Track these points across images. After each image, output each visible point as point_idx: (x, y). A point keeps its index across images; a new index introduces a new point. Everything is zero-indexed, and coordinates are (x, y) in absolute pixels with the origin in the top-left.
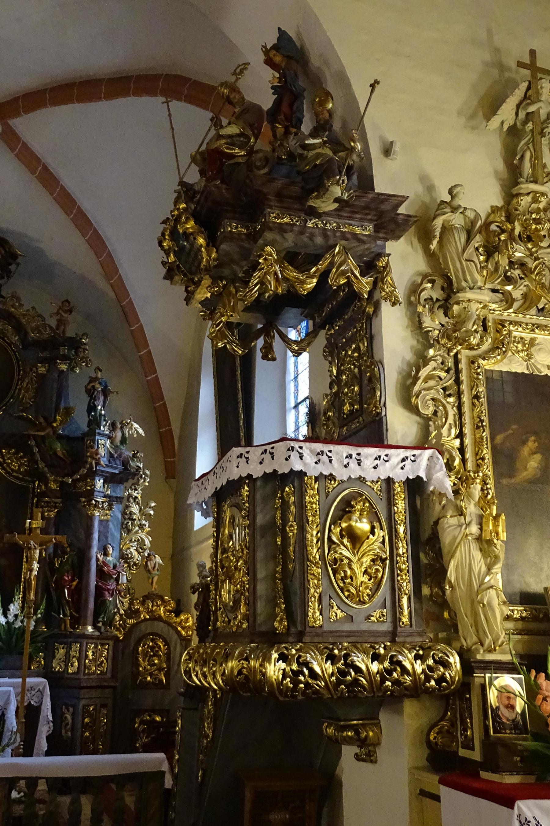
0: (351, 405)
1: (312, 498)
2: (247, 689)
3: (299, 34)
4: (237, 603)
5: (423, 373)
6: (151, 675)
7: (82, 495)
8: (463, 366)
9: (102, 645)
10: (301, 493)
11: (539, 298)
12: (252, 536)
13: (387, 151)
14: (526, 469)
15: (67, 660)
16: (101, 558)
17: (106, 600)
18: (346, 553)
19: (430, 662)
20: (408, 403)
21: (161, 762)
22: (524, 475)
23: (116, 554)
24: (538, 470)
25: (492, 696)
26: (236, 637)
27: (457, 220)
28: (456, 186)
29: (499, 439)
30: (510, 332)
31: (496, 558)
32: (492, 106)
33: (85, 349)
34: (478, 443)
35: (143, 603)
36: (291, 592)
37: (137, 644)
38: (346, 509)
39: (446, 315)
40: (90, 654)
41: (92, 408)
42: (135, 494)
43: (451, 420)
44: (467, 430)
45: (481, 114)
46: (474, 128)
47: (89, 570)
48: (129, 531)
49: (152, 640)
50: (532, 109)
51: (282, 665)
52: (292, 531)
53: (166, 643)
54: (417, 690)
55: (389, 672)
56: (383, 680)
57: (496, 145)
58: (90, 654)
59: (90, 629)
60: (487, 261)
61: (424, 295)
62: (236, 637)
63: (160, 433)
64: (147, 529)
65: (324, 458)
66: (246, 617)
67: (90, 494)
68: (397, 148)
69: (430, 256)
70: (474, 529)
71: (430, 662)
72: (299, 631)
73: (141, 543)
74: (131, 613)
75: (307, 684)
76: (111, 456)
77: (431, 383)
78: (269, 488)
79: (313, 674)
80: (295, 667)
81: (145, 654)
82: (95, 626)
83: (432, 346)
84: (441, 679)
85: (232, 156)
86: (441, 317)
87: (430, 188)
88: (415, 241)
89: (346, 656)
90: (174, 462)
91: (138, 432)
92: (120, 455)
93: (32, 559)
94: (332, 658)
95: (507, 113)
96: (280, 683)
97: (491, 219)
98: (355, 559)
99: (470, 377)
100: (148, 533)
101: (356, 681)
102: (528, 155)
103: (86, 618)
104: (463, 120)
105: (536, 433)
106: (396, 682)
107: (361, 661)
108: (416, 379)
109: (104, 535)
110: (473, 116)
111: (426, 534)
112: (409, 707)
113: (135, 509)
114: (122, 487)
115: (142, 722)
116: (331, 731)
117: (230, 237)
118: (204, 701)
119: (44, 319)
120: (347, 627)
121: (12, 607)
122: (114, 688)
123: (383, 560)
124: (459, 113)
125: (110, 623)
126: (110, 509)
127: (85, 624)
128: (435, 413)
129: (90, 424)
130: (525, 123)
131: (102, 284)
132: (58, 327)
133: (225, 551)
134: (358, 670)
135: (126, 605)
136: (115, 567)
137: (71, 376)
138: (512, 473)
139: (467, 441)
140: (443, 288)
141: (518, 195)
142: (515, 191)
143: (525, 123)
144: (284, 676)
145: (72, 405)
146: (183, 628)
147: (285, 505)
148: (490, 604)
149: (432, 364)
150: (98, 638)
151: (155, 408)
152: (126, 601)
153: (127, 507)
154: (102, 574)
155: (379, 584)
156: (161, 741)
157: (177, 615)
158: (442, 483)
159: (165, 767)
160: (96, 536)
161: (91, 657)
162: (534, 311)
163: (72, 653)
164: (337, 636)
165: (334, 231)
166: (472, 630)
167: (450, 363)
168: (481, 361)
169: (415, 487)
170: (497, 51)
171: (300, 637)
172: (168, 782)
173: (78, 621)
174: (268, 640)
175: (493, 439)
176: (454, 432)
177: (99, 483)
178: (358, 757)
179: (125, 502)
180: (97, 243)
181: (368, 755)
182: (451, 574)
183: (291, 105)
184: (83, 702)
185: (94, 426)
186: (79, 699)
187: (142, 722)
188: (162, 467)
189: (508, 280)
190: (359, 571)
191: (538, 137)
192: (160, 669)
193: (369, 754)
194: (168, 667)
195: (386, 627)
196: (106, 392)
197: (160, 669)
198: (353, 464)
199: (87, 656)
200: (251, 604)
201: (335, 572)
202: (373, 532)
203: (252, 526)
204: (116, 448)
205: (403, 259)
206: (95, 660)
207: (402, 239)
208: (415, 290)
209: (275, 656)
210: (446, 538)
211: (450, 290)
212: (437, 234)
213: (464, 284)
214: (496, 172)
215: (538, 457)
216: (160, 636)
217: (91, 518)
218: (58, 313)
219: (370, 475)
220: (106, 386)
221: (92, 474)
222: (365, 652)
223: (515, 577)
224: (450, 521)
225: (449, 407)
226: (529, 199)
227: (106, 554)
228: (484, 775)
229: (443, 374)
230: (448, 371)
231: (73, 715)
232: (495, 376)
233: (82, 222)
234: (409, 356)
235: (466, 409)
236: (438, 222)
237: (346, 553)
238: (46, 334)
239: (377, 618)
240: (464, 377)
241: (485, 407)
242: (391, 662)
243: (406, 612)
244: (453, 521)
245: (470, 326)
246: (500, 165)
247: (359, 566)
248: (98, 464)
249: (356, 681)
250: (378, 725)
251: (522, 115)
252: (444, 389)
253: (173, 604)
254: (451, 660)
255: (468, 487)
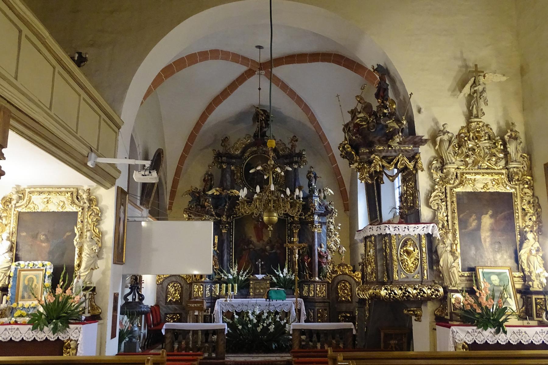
0: (411, 203)
1: (394, 242)
2: (375, 298)
3: (385, 64)
4: (372, 272)
5: (433, 195)
6: (344, 297)
7: (309, 222)
8: (448, 191)
9: (323, 285)
10: (390, 240)
11: (479, 162)
12: (376, 252)
13: (419, 111)
14: (471, 226)
15: (309, 291)
16: (319, 249)
17: (322, 267)
18: (405, 257)
19: (433, 290)
20: (428, 205)
21: (351, 326)
22: (470, 228)
23: (326, 247)
24: (500, 216)
25: (453, 301)
26: (372, 283)
27: (446, 137)
28: (445, 124)
29: (461, 216)
30: (466, 177)
31: (457, 257)
32: (462, 85)
33: (304, 157)
34: (453, 218)
35: (339, 267)
36: (388, 270)
37: (338, 285)
38: (405, 244)
39: (442, 172)
40: (318, 289)
41: (310, 185)
42: (331, 220)
43: (443, 210)
44: (449, 214)
45: (457, 89)
46: (454, 95)
47: (315, 255)
48: (330, 237)
49: (344, 283)
50: (475, 89)
51: (385, 291)
52: (388, 251)
53: (350, 284)
54: (429, 298)
55: (419, 293)
56: (417, 295)
57: (464, 102)
58: (318, 289)
59: (317, 279)
60: (458, 149)
61: (434, 166)
62: (372, 283)
63: (337, 179)
64: (338, 236)
65: (397, 229)
66: (375, 277)
67: (313, 222)
68: (423, 110)
69: (437, 151)
70: (449, 248)
71: (433, 290)
72: (391, 281)
73: (336, 242)
74: (334, 272)
75: (393, 297)
76: (320, 205)
77: (436, 198)
78: (380, 238)
79: (395, 294)
80: (389, 292)
81: (341, 289)
82: (319, 278)
83: (437, 185)
84: (437, 295)
85: (362, 125)
86: (440, 174)
87: (437, 123)
88: (431, 145)
89: (405, 289)
90: (348, 203)
91: (331, 193)
92: (324, 204)
93: (296, 253)
94: (401, 289)
95: (467, 90)
96: (385, 296)
97: (461, 132)
98: (408, 259)
99: (451, 195)
100: (338, 237)
101: (409, 296)
102: (475, 106)
103: (315, 274)
104: (450, 93)
105: (475, 213)
106: (421, 296)
107: (410, 290)
108: (431, 197)
109: (320, 239)
110: (454, 90)
111: (434, 250)
112: (429, 304)
113: (332, 227)
114: (326, 218)
115: (342, 316)
116: (406, 312)
117: (363, 153)
118: (365, 304)
119: (285, 145)
120: (406, 280)
121: (285, 270)
122: (329, 302)
123: (418, 259)
124: (449, 90)
125: (325, 276)
126: (321, 228)
127: (315, 277)
128: (438, 208)
129: (310, 191)
130: (474, 93)
131: (309, 124)
132: (292, 148)
133: (368, 255)
134: (409, 292)
135: (331, 268)
136: (325, 253)
137: (299, 169)
138: (466, 227)
139: (449, 218)
140: (441, 163)
141: (472, 122)
142: (470, 120)
143: (474, 93)
144: (386, 294)
145: (301, 185)
146: (357, 278)
147: (386, 243)
148: (453, 272)
149: (437, 191)
150: (321, 282)
151: (337, 179)
152: (331, 267)
153: (329, 226)
154: (320, 256)
155: (416, 267)
156: (352, 319)
157: (354, 272)
158: (436, 234)
159: (353, 327)
160: (316, 240)
161: (318, 290)
162: (476, 167)
163: (311, 289)
164: (403, 283)
165: (399, 150)
166: (448, 280)
167: (443, 190)
168: (454, 189)
169: (429, 236)
170: (465, 60)
171: (391, 283)
172: (354, 332)
173: (311, 276)
174: (383, 284)
175: (459, 216)
176: (445, 214)
177: (316, 217)
178: (415, 320)
179: (327, 224)
180: (306, 109)
181: (419, 320)
182: (441, 263)
183: (384, 93)
184: (317, 308)
185: (312, 193)
186: (315, 307)
187: (342, 316)
188: (343, 205)
189: (468, 156)
190: (410, 263)
191: (478, 99)
192: (348, 295)
193: (418, 319)
194: (351, 294)
195: (420, 280)
196: (315, 177)
197: (348, 295)
198: (406, 230)
199: (317, 290)
200: (377, 274)
201: (402, 263)
202: (414, 251)
203: (375, 249)
204: (322, 201)
205: (426, 153)
206: (320, 291)
207: (426, 145)
208: (430, 163)
209: (383, 288)
210: (439, 252)
211: (443, 164)
212: (438, 143)
213: (448, 162)
214: (463, 112)
215: (476, 221)
216: (347, 281)
217: (314, 232)
218: (291, 142)
219: (412, 234)
220: (315, 174)
221: (313, 214)
222: (412, 287)
223: (466, 263)
224: (441, 246)
225: (443, 206)
226: (476, 123)
227: (321, 247)
228: (450, 322)
229: (440, 194)
230: (442, 193)
231: (313, 313)
232: (460, 194)
233: (299, 101)
234: (429, 188)
235: (449, 207)
236: (438, 139)
237: (405, 257)
238: (287, 152)
239: (417, 277)
240: (448, 195)
241: (456, 205)
242: (420, 290)
243: (426, 275)
244: (442, 246)
245: (450, 177)
246: (465, 109)
247: (410, 262)
248: (315, 210)
249: (409, 296)
250: (421, 310)
251: (472, 90)
252: (441, 200)
253: (352, 268)
254: (440, 289)
255: (447, 235)
